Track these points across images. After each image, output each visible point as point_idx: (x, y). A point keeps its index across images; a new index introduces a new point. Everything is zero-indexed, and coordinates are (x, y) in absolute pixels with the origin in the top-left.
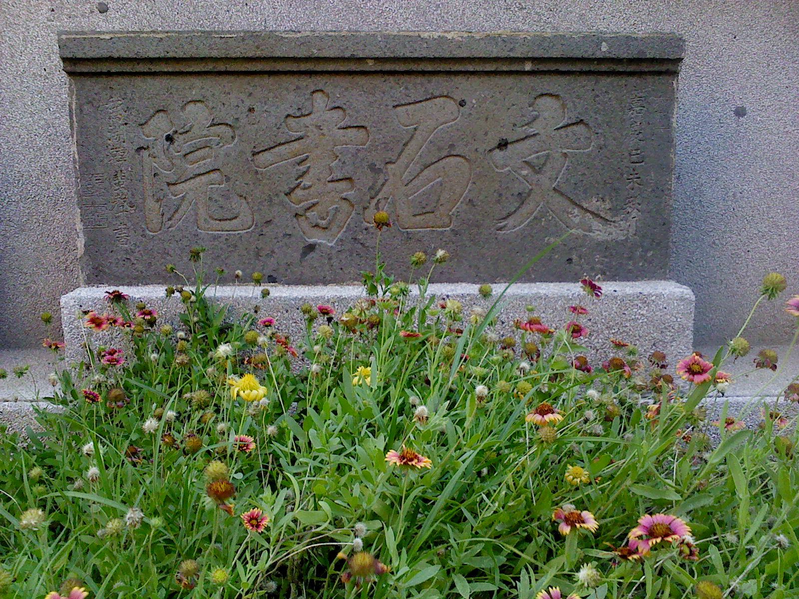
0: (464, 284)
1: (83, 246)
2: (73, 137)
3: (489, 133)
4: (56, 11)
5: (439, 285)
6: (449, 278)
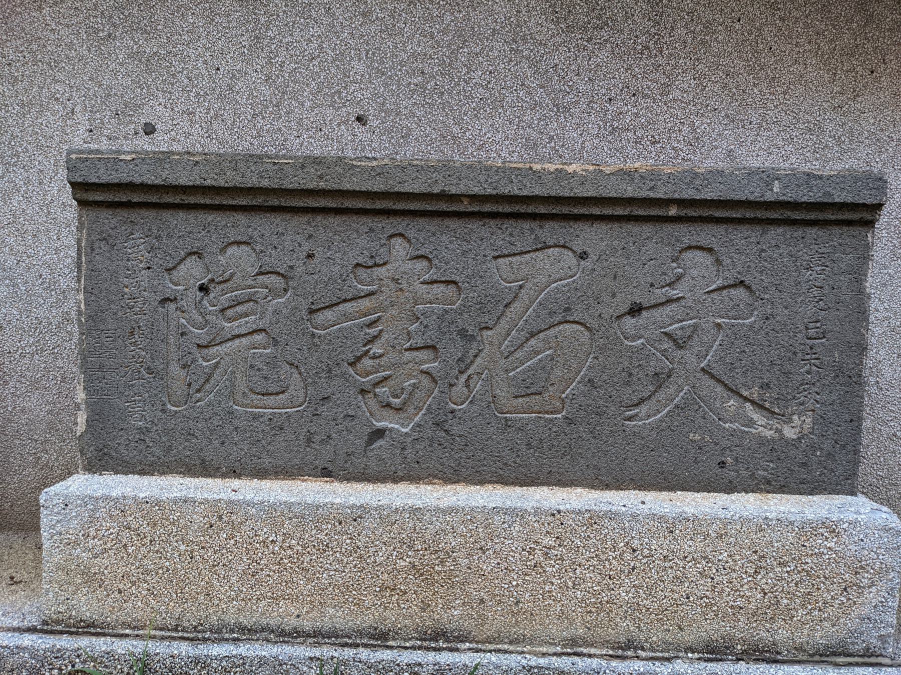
1: (84, 421)
5: (545, 488)
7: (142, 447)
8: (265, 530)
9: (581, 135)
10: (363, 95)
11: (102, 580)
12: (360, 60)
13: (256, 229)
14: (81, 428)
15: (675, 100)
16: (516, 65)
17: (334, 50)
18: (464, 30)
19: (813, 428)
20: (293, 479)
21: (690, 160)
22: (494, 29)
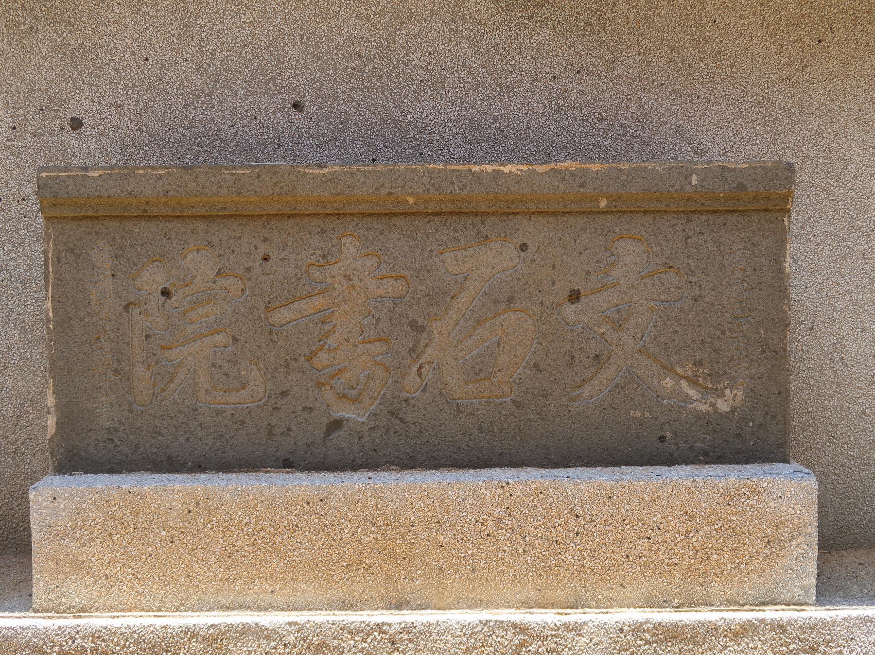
0: (529, 469)
1: (54, 424)
2: (47, 291)
3: (557, 283)
4: (18, 129)
5: (498, 469)
6: (510, 461)
7: (111, 446)
8: (240, 513)
9: (526, 114)
10: (298, 81)
11: (89, 567)
12: (294, 46)
13: (214, 235)
14: (51, 429)
15: (620, 76)
16: (456, 45)
17: (267, 36)
18: (402, 12)
19: (745, 400)
20: (256, 471)
21: (639, 136)
22: (431, 10)
